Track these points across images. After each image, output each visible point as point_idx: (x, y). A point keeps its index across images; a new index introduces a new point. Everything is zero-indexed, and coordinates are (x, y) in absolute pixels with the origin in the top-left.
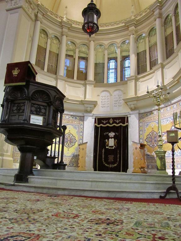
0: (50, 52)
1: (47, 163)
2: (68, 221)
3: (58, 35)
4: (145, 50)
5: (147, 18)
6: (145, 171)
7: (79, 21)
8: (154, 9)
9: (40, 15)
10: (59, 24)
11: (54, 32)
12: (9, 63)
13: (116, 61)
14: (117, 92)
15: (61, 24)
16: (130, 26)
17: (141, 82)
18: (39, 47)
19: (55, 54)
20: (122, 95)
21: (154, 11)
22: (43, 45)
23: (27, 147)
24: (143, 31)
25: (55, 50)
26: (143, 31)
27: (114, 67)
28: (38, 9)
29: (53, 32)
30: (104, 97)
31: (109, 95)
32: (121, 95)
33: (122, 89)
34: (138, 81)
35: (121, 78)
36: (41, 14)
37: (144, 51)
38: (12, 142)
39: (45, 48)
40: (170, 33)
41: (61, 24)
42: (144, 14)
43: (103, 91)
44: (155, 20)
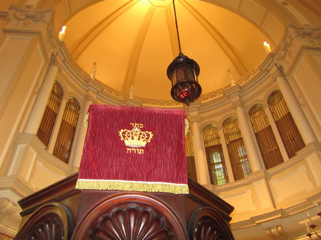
0: (63, 121)
2: (137, 136)
4: (288, 114)
5: (269, 65)
7: (112, 88)
9: (59, 59)
10: (84, 83)
12: (232, 220)
13: (266, 68)
15: (87, 83)
18: (48, 109)
19: (68, 125)
21: (268, 69)
22: (53, 107)
23: (38, 196)
25: (70, 119)
28: (60, 49)
29: (73, 91)
35: (313, 196)
36: (61, 58)
37: (286, 115)
39: (55, 113)
40: (282, 116)
41: (87, 83)
44: (275, 80)
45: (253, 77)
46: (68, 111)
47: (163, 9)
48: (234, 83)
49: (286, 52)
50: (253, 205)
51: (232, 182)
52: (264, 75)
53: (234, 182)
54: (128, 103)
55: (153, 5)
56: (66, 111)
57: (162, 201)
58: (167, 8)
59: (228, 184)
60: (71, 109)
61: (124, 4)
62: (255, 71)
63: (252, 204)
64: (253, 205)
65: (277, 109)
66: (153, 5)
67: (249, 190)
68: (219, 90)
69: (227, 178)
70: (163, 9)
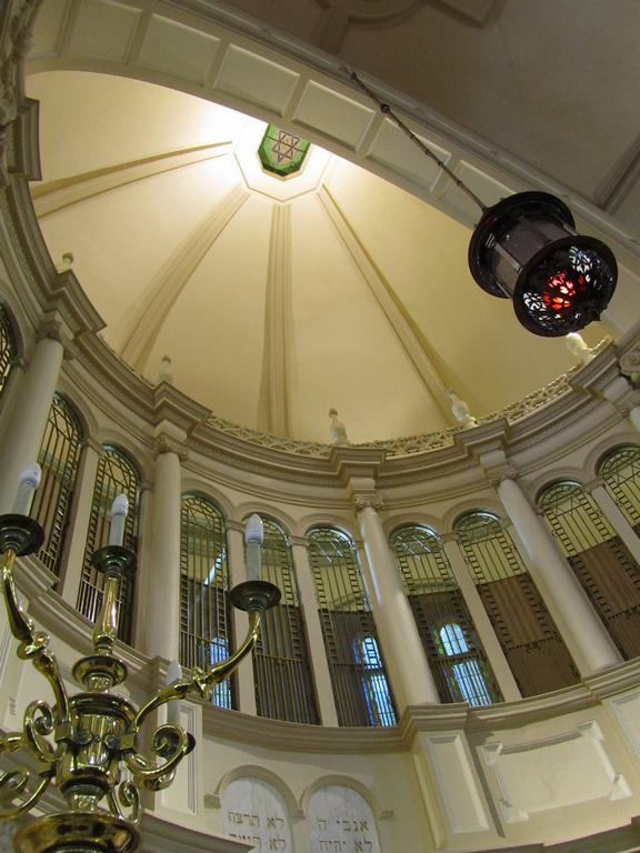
1: (27, 602)
3: (134, 444)
6: (121, 821)
8: (596, 382)
11: (117, 428)
14: (333, 799)
16: (483, 449)
17: (505, 752)
20: (371, 825)
24: (424, 509)
26: (424, 509)
27: (459, 669)
30: (246, 821)
31: (278, 809)
32: (364, 825)
33: (367, 779)
34: (482, 742)
38: (14, 626)
42: (550, 402)
43: (243, 773)
45: (535, 411)
46: (62, 465)
47: (271, 202)
48: (473, 423)
49: (182, 444)
50: (617, 779)
51: (512, 701)
52: (581, 402)
53: (522, 702)
54: (468, 447)
55: (247, 183)
56: (184, 559)
57: (65, 626)
58: (282, 204)
59: (502, 706)
60: (115, 480)
61: (148, 156)
62: (541, 396)
63: (612, 775)
64: (617, 779)
65: (51, 496)
66: (247, 183)
67: (590, 724)
68: (406, 440)
69: (495, 692)
70: (271, 202)
